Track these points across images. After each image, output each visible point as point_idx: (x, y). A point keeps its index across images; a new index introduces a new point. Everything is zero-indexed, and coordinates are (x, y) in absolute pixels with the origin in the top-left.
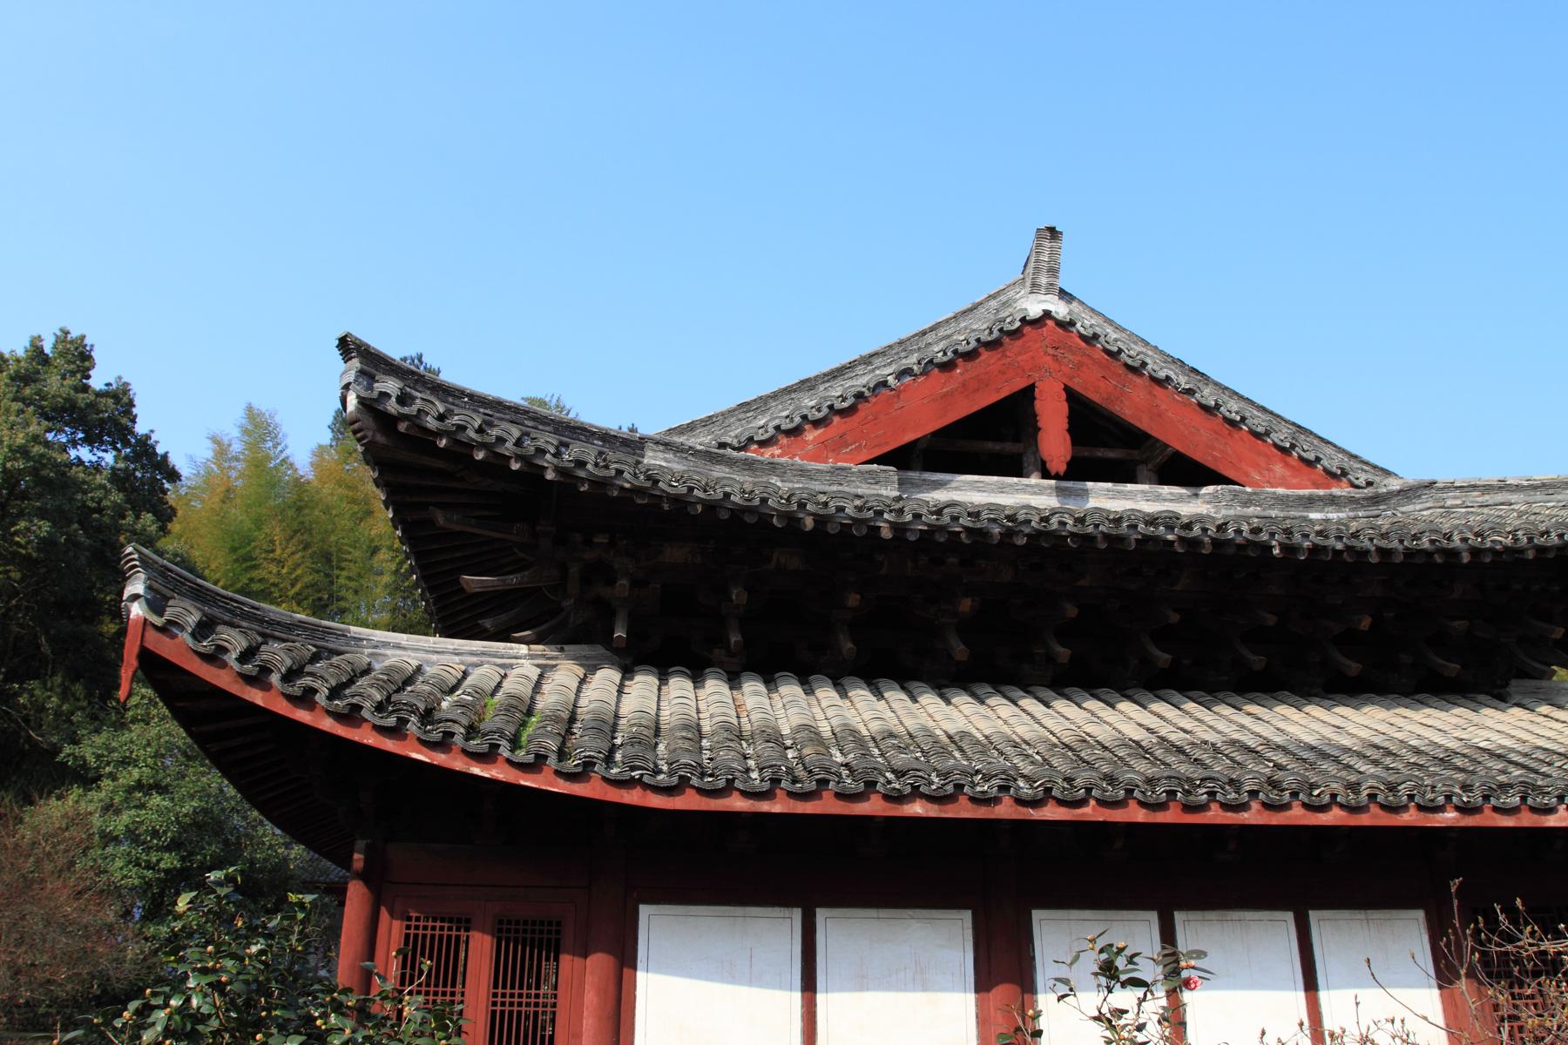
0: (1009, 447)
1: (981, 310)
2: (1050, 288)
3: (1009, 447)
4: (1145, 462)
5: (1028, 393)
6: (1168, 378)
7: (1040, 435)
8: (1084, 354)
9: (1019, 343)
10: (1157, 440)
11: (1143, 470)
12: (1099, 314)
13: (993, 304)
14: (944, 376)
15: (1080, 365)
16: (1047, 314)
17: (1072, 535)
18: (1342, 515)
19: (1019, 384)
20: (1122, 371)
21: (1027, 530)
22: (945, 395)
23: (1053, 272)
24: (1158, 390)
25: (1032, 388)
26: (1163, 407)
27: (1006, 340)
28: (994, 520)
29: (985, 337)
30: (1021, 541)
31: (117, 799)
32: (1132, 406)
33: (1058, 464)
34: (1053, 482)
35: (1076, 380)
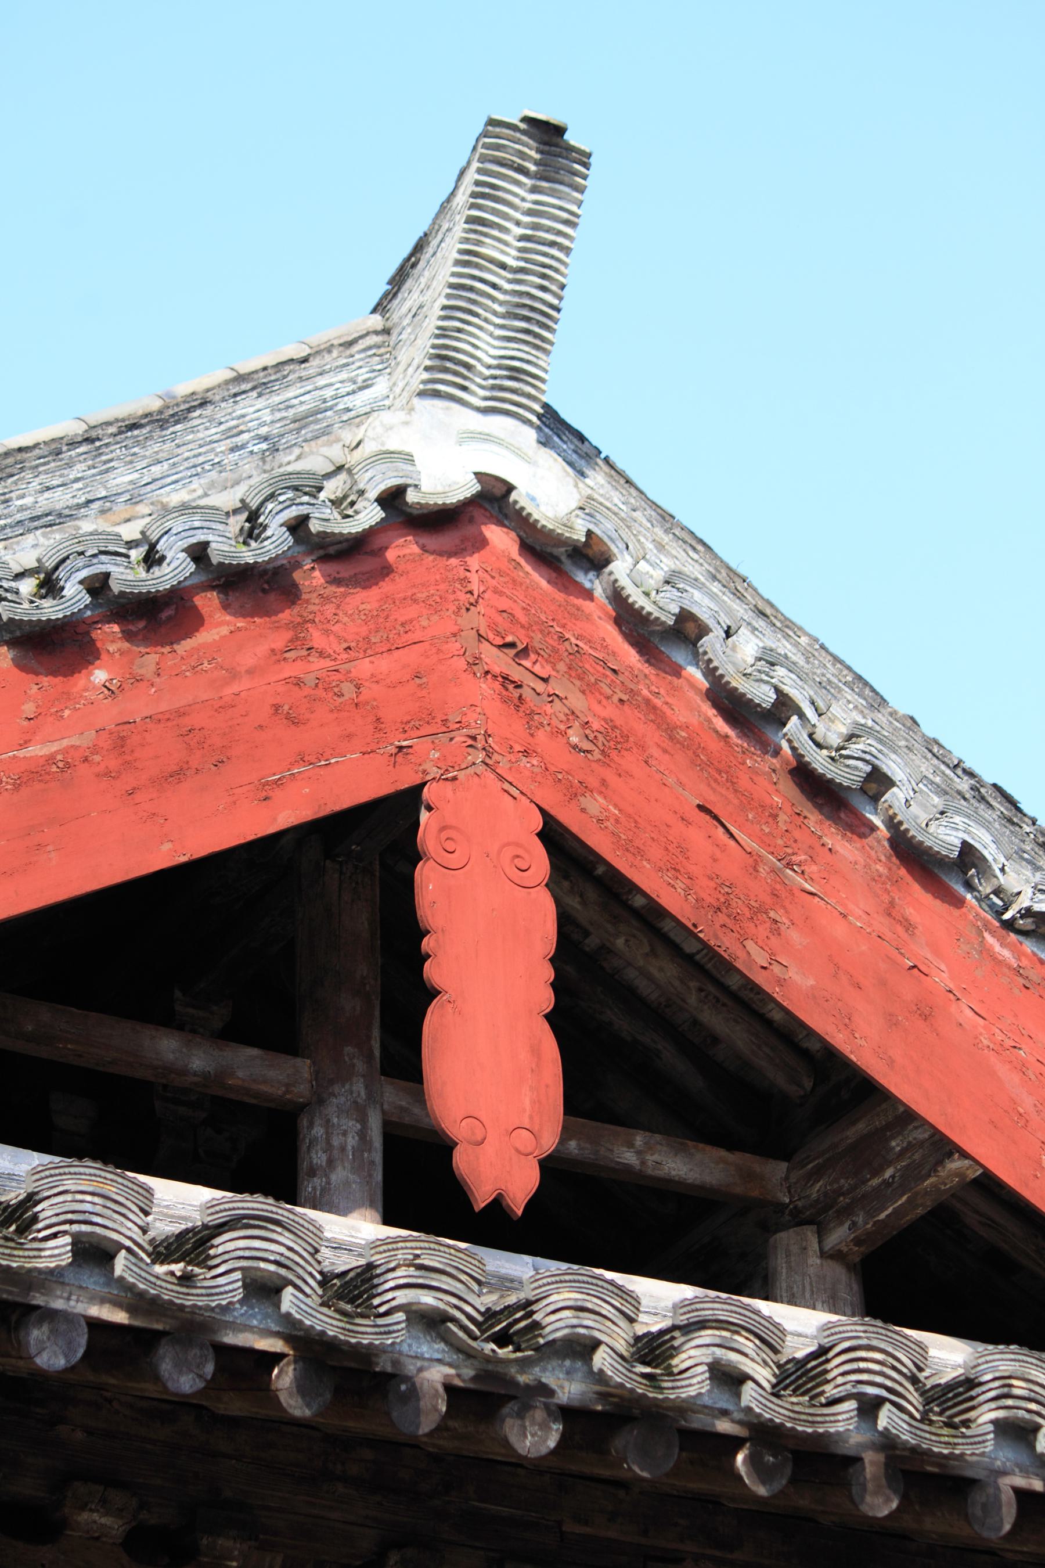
0: (254, 1070)
1: (202, 429)
2: (512, 390)
3: (254, 1070)
4: (815, 1218)
5: (379, 839)
6: (969, 857)
7: (546, 999)
8: (631, 699)
9: (364, 600)
10: (909, 1117)
11: (799, 1251)
12: (696, 543)
13: (257, 411)
14: (36, 690)
15: (613, 741)
16: (494, 498)
17: (763, 1434)
19: (354, 781)
20: (784, 794)
21: (569, 1387)
22: (36, 774)
23: (534, 319)
24: (918, 901)
25: (407, 803)
26: (942, 978)
27: (312, 578)
28: (431, 1322)
29: (227, 547)
30: (536, 1438)
32: (823, 952)
33: (501, 1166)
35: (594, 804)
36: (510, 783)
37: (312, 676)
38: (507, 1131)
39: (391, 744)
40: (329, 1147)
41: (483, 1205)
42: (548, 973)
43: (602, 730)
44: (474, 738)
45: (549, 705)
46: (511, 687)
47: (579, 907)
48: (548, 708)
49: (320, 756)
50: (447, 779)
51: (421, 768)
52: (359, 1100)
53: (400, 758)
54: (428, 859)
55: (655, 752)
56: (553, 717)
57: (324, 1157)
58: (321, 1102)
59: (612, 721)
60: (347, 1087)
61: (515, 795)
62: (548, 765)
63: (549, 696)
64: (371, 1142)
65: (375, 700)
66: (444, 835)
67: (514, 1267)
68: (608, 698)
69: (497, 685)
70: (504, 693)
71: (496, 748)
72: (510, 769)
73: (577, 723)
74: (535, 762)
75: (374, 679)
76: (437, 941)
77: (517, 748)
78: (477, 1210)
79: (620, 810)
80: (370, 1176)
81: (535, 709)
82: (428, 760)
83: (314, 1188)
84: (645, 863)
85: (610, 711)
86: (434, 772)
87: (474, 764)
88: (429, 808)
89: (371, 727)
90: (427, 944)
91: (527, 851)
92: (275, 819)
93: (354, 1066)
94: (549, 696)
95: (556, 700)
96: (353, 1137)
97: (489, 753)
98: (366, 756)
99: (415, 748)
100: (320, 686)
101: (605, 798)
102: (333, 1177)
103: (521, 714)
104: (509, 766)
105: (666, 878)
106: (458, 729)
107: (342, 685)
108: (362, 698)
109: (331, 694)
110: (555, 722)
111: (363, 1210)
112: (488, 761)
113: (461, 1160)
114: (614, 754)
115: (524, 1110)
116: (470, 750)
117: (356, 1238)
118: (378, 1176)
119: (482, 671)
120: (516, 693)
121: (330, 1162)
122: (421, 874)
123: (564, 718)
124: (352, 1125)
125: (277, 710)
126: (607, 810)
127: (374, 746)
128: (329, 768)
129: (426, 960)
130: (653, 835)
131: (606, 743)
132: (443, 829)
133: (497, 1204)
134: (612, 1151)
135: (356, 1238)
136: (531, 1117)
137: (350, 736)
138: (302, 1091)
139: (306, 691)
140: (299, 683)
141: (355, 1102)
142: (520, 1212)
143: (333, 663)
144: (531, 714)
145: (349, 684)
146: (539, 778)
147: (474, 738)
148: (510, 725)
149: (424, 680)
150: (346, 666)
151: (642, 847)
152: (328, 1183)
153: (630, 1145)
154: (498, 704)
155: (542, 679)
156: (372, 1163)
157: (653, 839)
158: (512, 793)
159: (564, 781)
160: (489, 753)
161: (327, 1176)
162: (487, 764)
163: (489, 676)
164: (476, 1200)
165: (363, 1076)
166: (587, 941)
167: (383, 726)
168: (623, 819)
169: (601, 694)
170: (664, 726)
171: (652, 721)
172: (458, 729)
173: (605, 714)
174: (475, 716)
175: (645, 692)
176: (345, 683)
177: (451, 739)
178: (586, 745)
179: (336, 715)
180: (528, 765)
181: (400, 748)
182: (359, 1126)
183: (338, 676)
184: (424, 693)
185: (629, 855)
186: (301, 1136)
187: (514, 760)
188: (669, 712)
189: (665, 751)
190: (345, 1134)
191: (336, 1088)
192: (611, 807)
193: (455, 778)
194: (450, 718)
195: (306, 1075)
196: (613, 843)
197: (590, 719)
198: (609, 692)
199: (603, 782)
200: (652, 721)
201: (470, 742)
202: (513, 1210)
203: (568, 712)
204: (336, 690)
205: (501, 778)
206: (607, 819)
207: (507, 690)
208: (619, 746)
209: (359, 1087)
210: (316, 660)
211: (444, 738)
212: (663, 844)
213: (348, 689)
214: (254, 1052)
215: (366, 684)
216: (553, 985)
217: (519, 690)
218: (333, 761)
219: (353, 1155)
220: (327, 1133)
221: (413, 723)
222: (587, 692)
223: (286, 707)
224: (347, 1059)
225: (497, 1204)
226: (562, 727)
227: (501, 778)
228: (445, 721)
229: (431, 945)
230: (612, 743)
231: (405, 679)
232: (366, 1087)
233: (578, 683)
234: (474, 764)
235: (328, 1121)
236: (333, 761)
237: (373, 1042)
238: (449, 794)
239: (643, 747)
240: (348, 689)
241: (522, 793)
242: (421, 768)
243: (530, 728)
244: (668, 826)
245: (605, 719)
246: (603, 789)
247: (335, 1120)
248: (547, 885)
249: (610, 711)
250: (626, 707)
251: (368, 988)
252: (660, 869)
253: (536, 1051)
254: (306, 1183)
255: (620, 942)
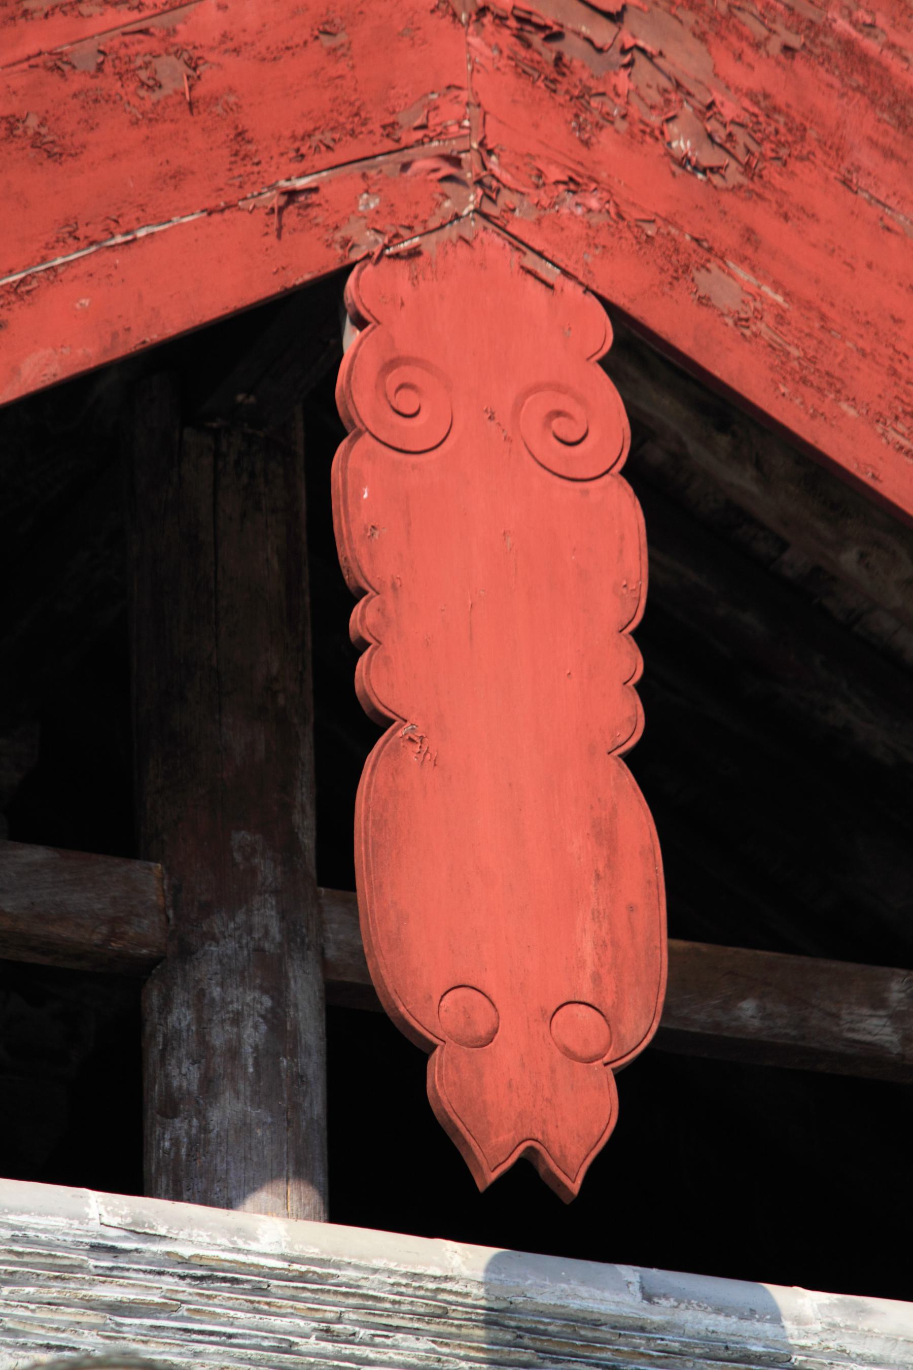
5: (260, 387)
7: (627, 720)
18: (84, 1292)
19: (195, 273)
25: (312, 315)
31: (164, 991)
33: (535, 1081)
34: (461, 1264)
35: (730, 286)
36: (540, 254)
37: (90, 47)
38: (543, 1011)
39: (271, 187)
40: (203, 1051)
41: (494, 1176)
42: (630, 662)
43: (746, 118)
44: (456, 162)
45: (623, 74)
46: (537, 39)
47: (754, 489)
48: (622, 80)
49: (113, 224)
50: (397, 256)
51: (338, 236)
52: (267, 946)
53: (291, 217)
54: (359, 434)
55: (866, 158)
56: (634, 98)
57: (195, 1074)
58: (186, 953)
59: (766, 96)
60: (240, 918)
61: (551, 279)
62: (624, 208)
63: (624, 51)
64: (296, 1032)
65: (231, 90)
66: (394, 379)
67: (598, 1294)
68: (757, 46)
69: (506, 38)
70: (523, 53)
71: (506, 177)
72: (539, 221)
73: (688, 109)
74: (594, 203)
75: (230, 45)
76: (381, 611)
77: (554, 173)
78: (481, 1187)
79: (787, 295)
80: (296, 1107)
81: (592, 83)
82: (357, 213)
83: (176, 1142)
84: (844, 406)
85: (762, 75)
86: (369, 242)
87: (457, 217)
88: (360, 323)
89: (226, 152)
90: (362, 619)
91: (580, 400)
92: (15, 370)
93: (253, 871)
94: (624, 51)
95: (640, 59)
96: (256, 1027)
97: (489, 189)
98: (216, 217)
99: (324, 191)
100: (108, 68)
101: (753, 269)
102: (215, 1116)
103: (561, 98)
104: (534, 215)
105: (892, 435)
106: (421, 142)
107: (157, 63)
108: (201, 90)
109: (132, 86)
110: (637, 109)
111: (280, 1186)
112: (488, 208)
113: (444, 1082)
114: (772, 171)
115: (582, 964)
116: (448, 187)
117: (248, 1252)
118: (315, 1104)
119: (473, 9)
120: (548, 53)
121: (208, 1084)
122: (344, 469)
123: (657, 99)
124: (253, 1000)
125: (11, 129)
126: (757, 296)
127: (231, 195)
128: (134, 249)
129: (360, 654)
130: (861, 343)
131: (753, 147)
132: (390, 365)
133: (526, 1172)
134: (836, 1016)
135: (248, 1252)
136: (597, 979)
137: (177, 177)
138: (146, 932)
139: (77, 82)
140: (58, 64)
141: (259, 950)
142: (575, 1187)
143: (135, 15)
144: (582, 98)
145: (173, 58)
146: (603, 238)
147: (456, 162)
148: (536, 125)
149: (342, 38)
150: (165, 18)
151: (837, 372)
152: (204, 1129)
153: (878, 1002)
154: (509, 78)
155: (608, 15)
156: (300, 1078)
157: (863, 353)
158: (543, 275)
159: (659, 240)
160: (489, 189)
161: (201, 1114)
162: (486, 216)
163: (488, 19)
164: (480, 1167)
165: (275, 892)
166: (787, 556)
167: (252, 147)
168: (793, 313)
169: (741, 37)
170: (887, 99)
171: (858, 89)
172: (421, 142)
173: (749, 81)
174: (458, 110)
175: (842, 25)
176: (165, 59)
177: (405, 166)
178: (709, 156)
179: (144, 131)
180: (579, 211)
181: (292, 195)
182: (267, 1002)
183: (148, 44)
184: (342, 67)
185: (808, 391)
186: (148, 1029)
187: (545, 202)
188: (896, 65)
189: (889, 154)
190: (237, 1019)
191: (217, 923)
192: (767, 289)
193: (415, 253)
194: (402, 118)
195: (154, 898)
196: (772, 368)
197: (718, 97)
198: (760, 31)
199: (749, 235)
200: (858, 89)
201: (447, 169)
202: (561, 1184)
203: (665, 83)
204: (143, 75)
205: (519, 244)
206: (759, 315)
207: (528, 45)
208: (783, 152)
209: (266, 917)
210: (96, 10)
211: (388, 165)
212: (887, 363)
213: (171, 72)
214: (38, 854)
215: (212, 57)
216: (642, 688)
217: (556, 46)
218: (141, 233)
219: (256, 1064)
220: (199, 1020)
221: (318, 136)
222: (711, 36)
223: (33, 122)
224: (238, 857)
225: (526, 1172)
226: (655, 119)
227: (519, 244)
228: (390, 128)
229: (369, 621)
230: (767, 148)
231: (298, 40)
232: (283, 915)
233: (689, 17)
234: (457, 217)
235: (202, 993)
236: (141, 233)
237: (297, 818)
238: (404, 288)
239: (837, 149)
240: (171, 72)
241: (565, 272)
242: (338, 236)
243: (581, 128)
244: (897, 321)
245: (751, 95)
246: (749, 251)
247: (216, 992)
248: (624, 472)
249: (762, 75)
250: (799, 65)
251: (281, 700)
252: (879, 418)
253: (605, 835)
254: (158, 1130)
255: (848, 559)
